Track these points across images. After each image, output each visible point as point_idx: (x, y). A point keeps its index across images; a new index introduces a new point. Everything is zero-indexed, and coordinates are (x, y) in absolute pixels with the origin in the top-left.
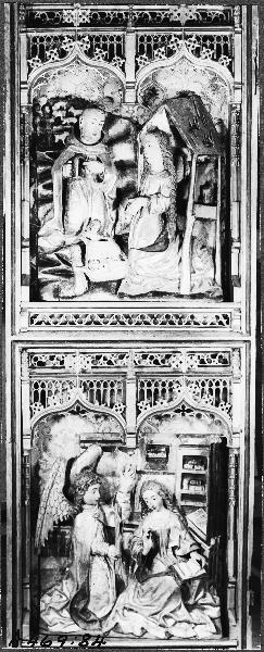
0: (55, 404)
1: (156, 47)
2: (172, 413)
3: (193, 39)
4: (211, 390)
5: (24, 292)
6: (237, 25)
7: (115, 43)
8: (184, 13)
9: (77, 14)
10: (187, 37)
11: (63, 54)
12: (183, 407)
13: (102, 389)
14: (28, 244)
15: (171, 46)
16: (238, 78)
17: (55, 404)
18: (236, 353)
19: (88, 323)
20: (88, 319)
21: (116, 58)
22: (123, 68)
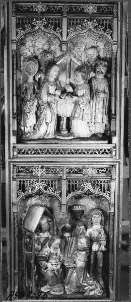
0: (29, 191)
1: (26, 23)
2: (83, 195)
3: (44, 20)
4: (98, 185)
5: (13, 140)
6: (115, 14)
7: (108, 23)
8: (40, 7)
9: (91, 9)
10: (41, 19)
11: (33, 26)
12: (39, 192)
13: (103, 184)
14: (15, 116)
15: (33, 23)
16: (115, 39)
17: (29, 191)
18: (114, 168)
19: (91, 153)
20: (103, 151)
21: (108, 30)
22: (111, 35)
